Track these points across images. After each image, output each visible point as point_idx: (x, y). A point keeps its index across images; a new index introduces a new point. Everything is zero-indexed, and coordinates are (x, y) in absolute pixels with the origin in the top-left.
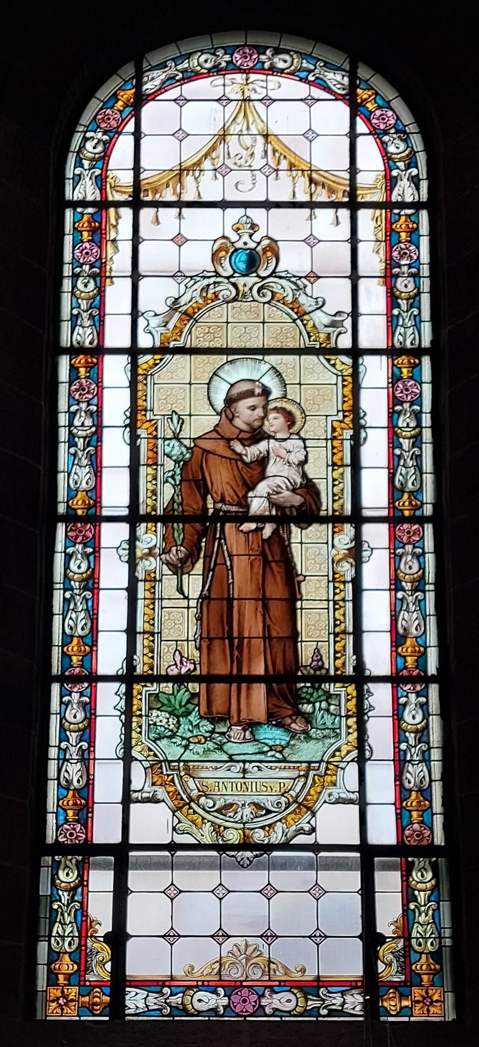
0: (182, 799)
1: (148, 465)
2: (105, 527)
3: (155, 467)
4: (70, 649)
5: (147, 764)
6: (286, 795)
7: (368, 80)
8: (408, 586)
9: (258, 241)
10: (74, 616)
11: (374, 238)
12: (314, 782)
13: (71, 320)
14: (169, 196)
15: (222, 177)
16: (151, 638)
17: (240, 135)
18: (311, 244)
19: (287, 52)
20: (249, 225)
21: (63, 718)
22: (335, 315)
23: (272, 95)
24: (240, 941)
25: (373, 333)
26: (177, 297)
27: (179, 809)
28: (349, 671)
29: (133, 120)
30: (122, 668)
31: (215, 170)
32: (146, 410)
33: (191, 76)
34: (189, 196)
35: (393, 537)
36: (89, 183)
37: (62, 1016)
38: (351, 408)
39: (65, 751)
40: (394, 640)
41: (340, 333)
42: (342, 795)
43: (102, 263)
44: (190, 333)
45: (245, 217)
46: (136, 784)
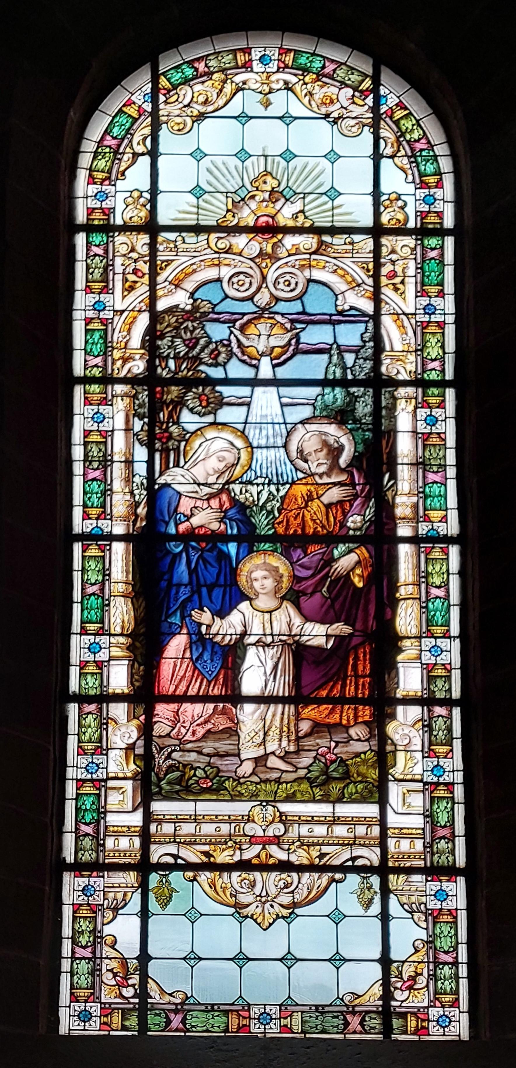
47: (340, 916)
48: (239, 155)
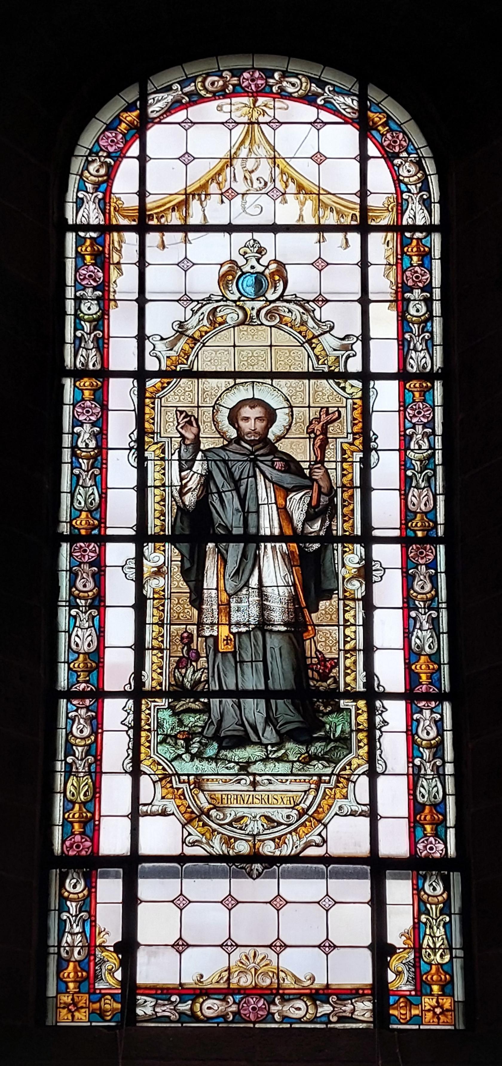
0: (192, 812)
1: (156, 487)
2: (110, 547)
3: (162, 488)
4: (418, 667)
5: (155, 778)
6: (297, 807)
7: (380, 103)
9: (266, 264)
10: (80, 633)
14: (174, 219)
16: (160, 655)
19: (296, 76)
20: (256, 250)
22: (343, 339)
24: (250, 952)
25: (385, 358)
26: (183, 320)
27: (190, 821)
28: (360, 688)
29: (137, 142)
32: (153, 433)
33: (196, 99)
34: (195, 219)
35: (405, 557)
36: (92, 206)
37: (73, 1021)
38: (360, 431)
39: (71, 765)
40: (407, 657)
41: (348, 357)
42: (354, 808)
45: (252, 241)
46: (145, 797)
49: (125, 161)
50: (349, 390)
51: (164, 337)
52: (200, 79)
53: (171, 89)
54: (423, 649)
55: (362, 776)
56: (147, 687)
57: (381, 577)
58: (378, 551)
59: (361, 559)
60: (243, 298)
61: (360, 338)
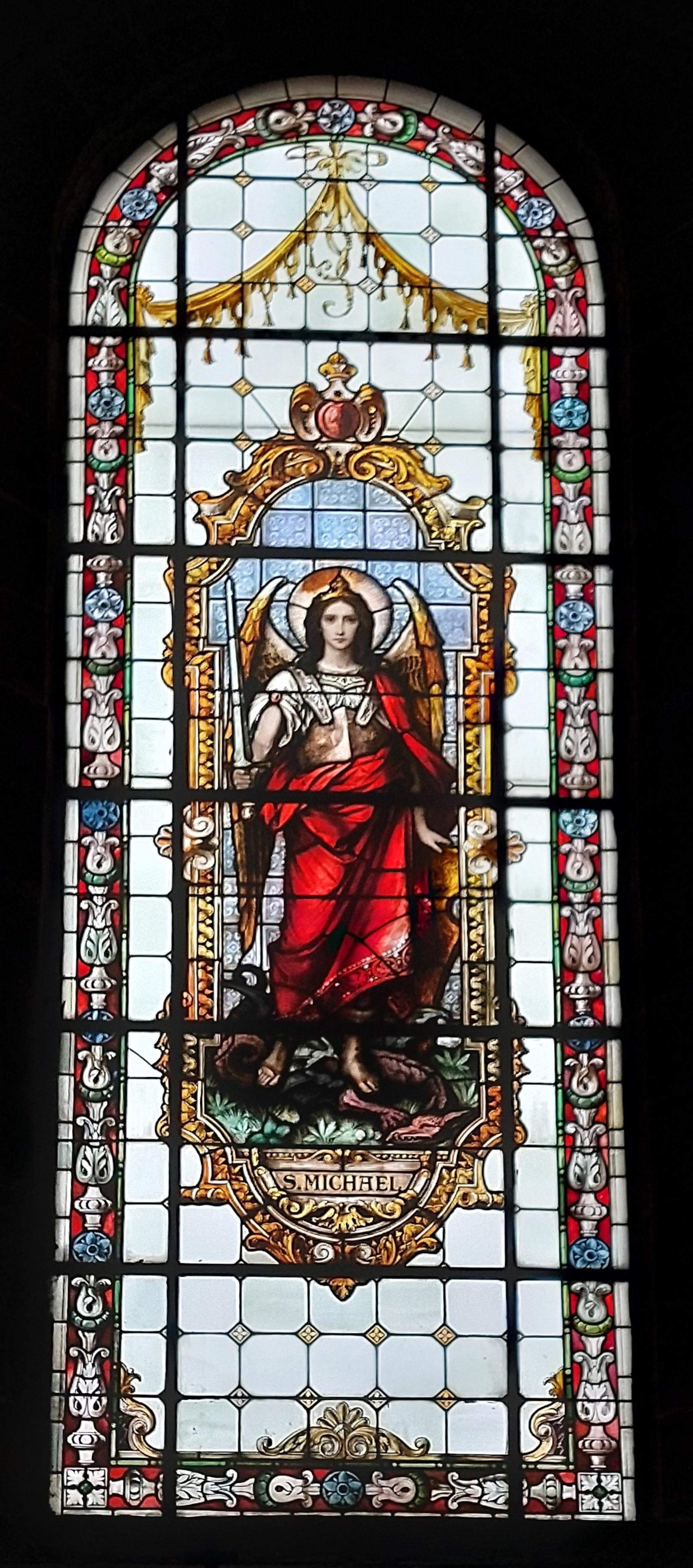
0: (254, 1200)
1: (200, 718)
3: (210, 721)
8: (577, 898)
9: (356, 389)
11: (524, 390)
12: (441, 1178)
13: (85, 504)
14: (225, 320)
15: (303, 295)
17: (328, 232)
18: (433, 394)
21: (79, 1082)
23: (375, 173)
24: (333, 1405)
25: (525, 531)
26: (238, 469)
27: (252, 1214)
29: (175, 205)
30: (164, 1010)
31: (293, 284)
33: (254, 142)
34: (254, 322)
41: (473, 529)
42: (483, 1198)
43: (128, 420)
44: (260, 526)
47: (313, 1334)
48: (424, 234)
49: (156, 233)
50: (475, 579)
51: (213, 494)
52: (260, 114)
53: (219, 128)
54: (580, 963)
55: (494, 1152)
56: (194, 1014)
57: (521, 855)
58: (516, 818)
59: (491, 828)
60: (324, 439)
61: (490, 501)
